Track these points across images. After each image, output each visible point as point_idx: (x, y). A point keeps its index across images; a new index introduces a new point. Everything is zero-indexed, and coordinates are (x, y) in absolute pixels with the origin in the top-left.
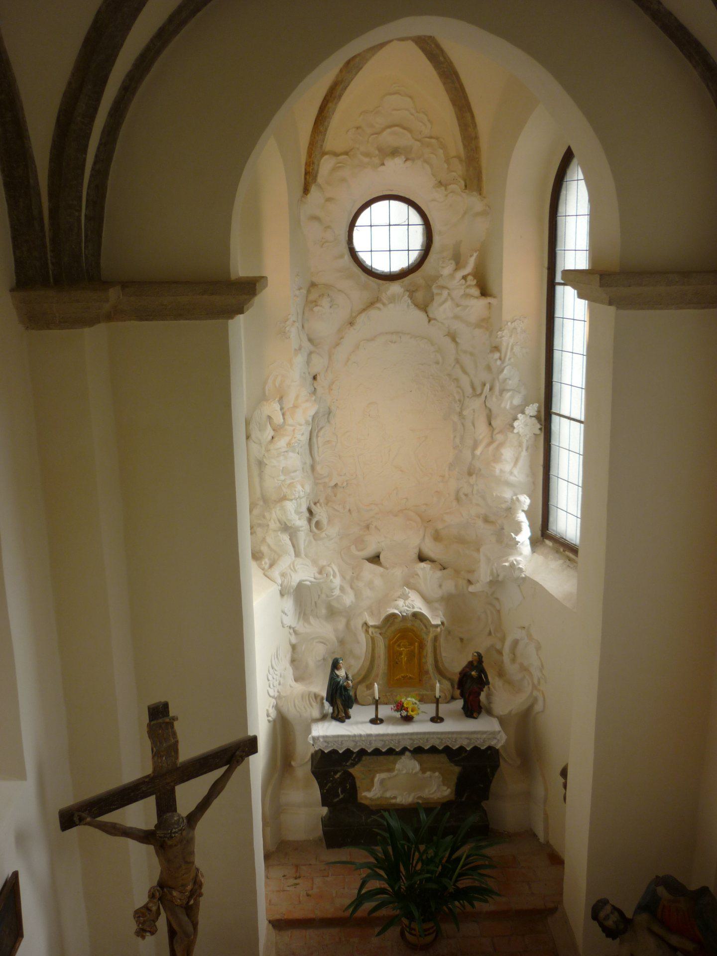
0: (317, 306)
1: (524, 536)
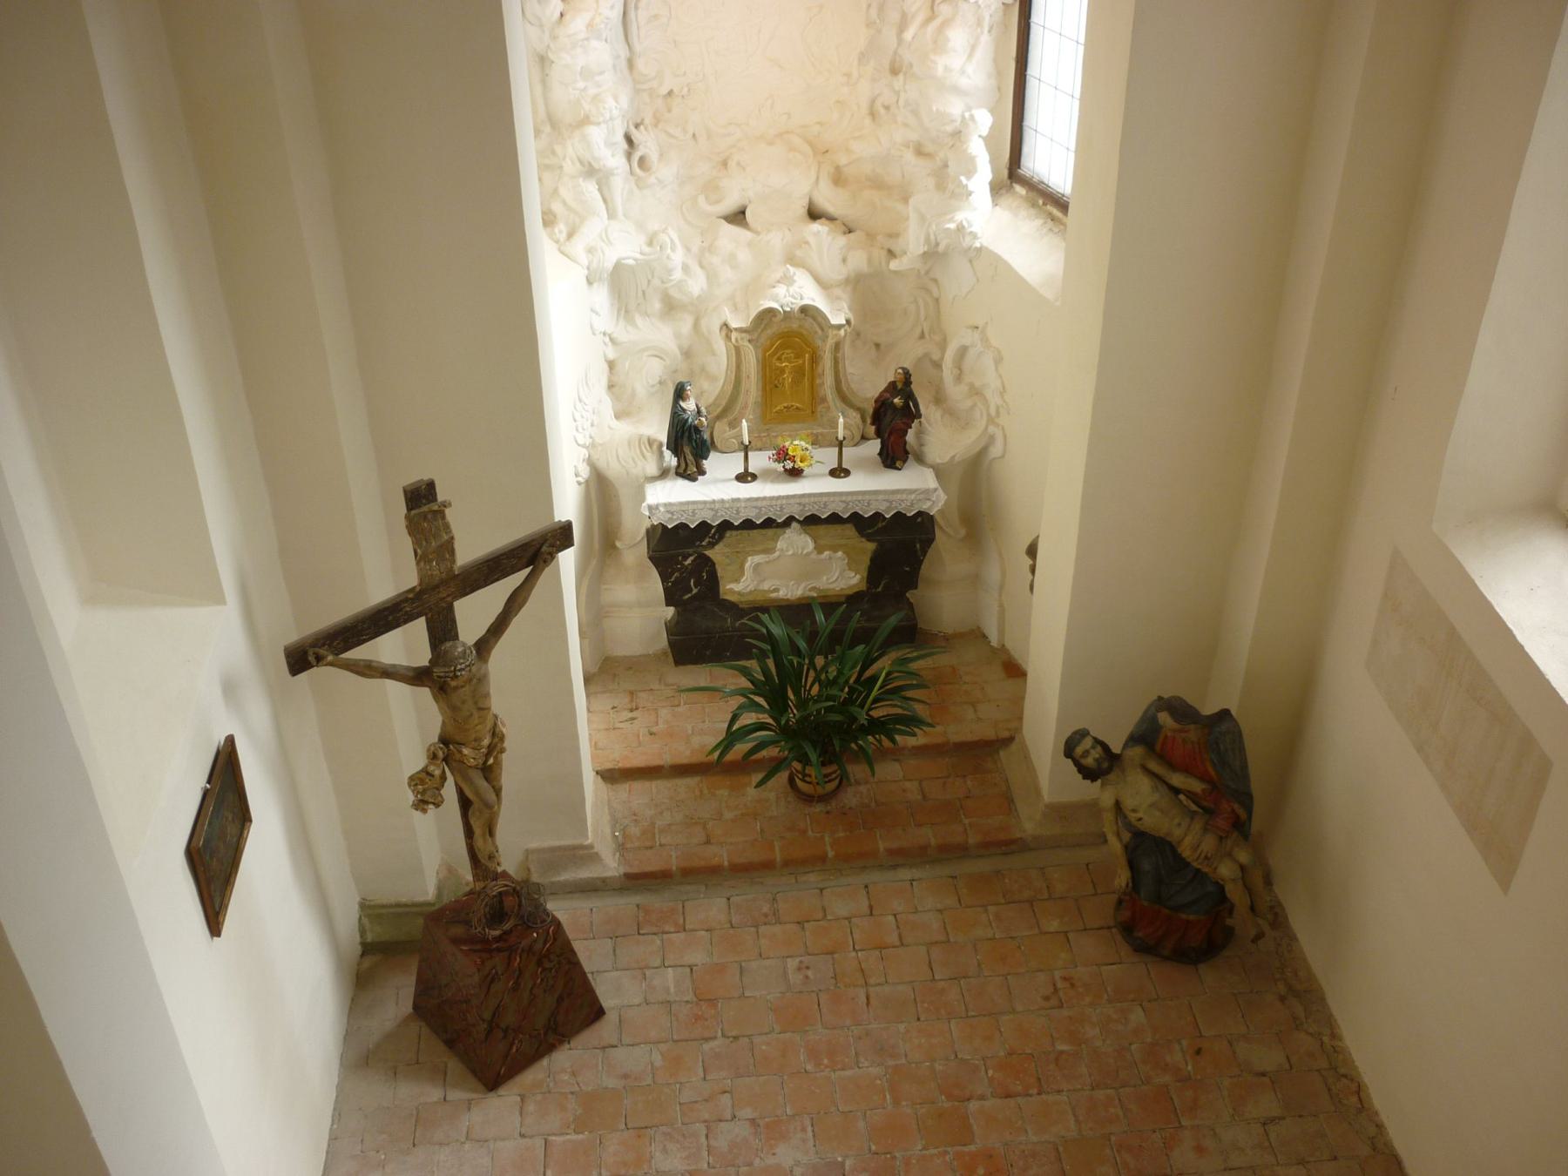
1: (981, 180)
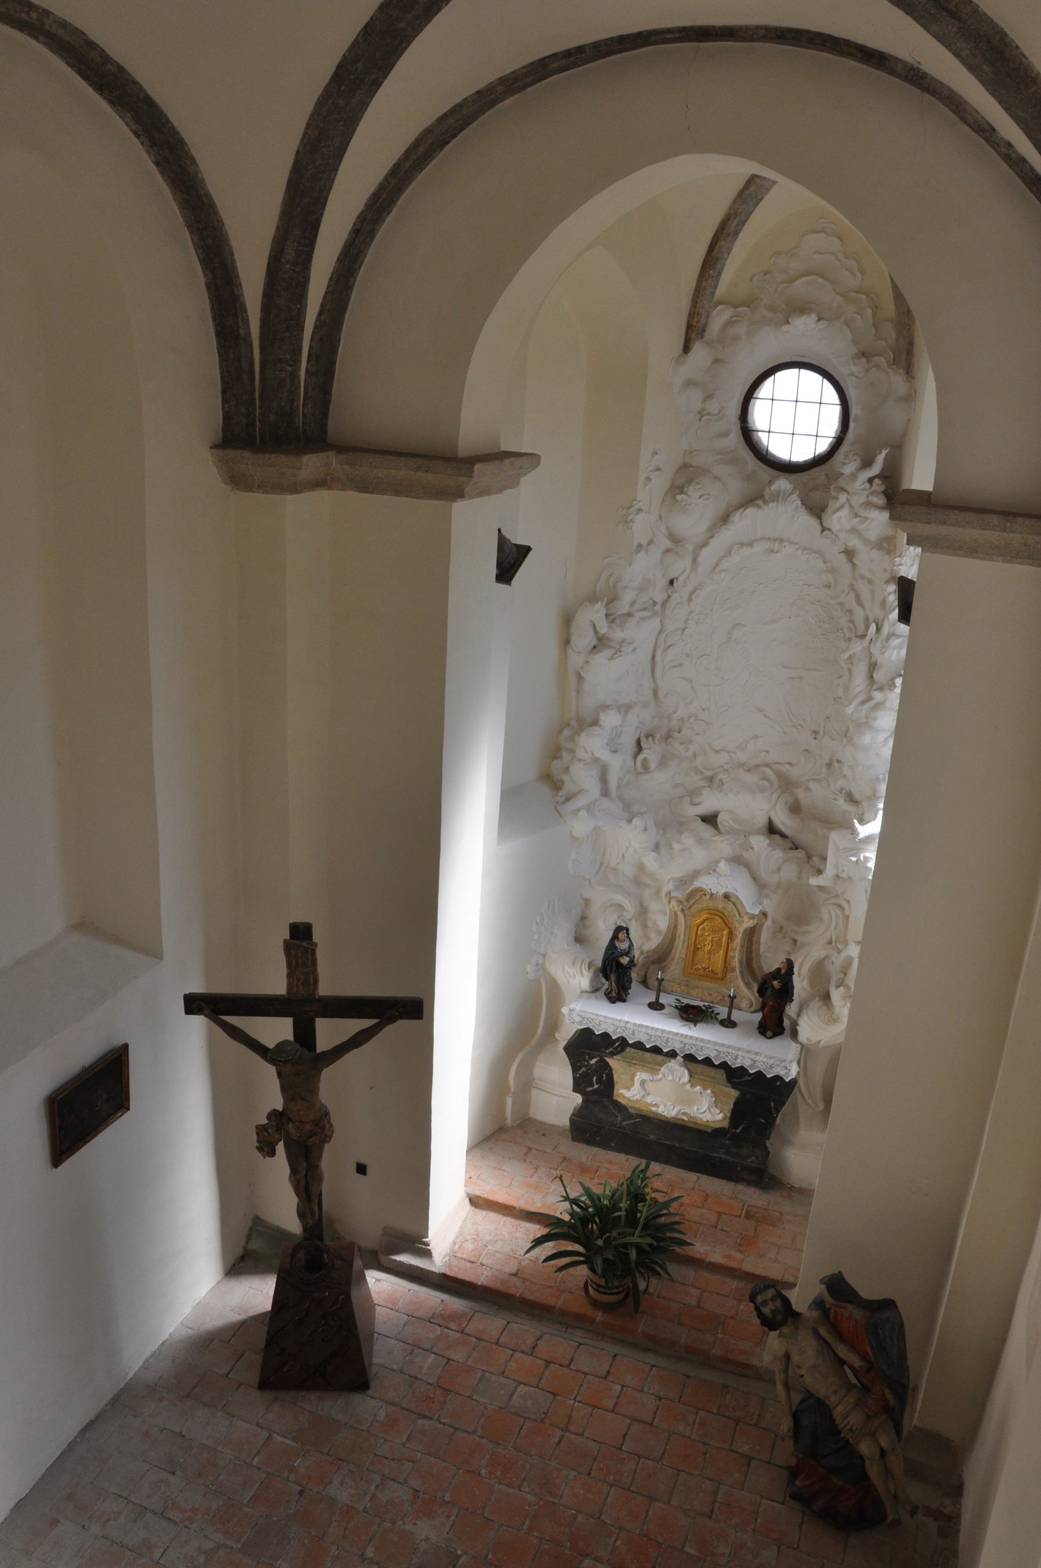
0: (682, 493)
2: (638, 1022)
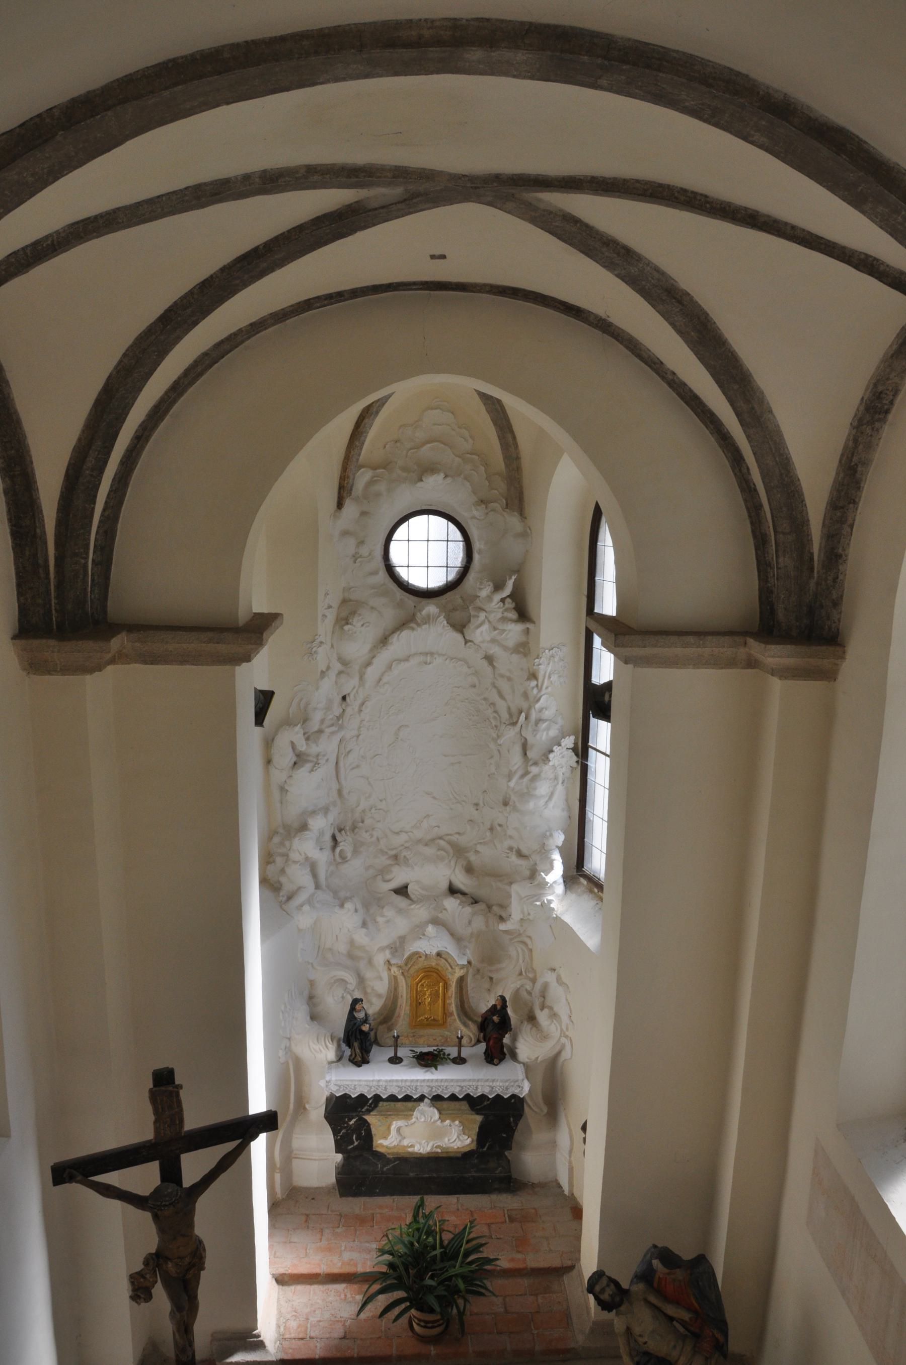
0: (347, 624)
1: (555, 874)
2: (388, 1078)
